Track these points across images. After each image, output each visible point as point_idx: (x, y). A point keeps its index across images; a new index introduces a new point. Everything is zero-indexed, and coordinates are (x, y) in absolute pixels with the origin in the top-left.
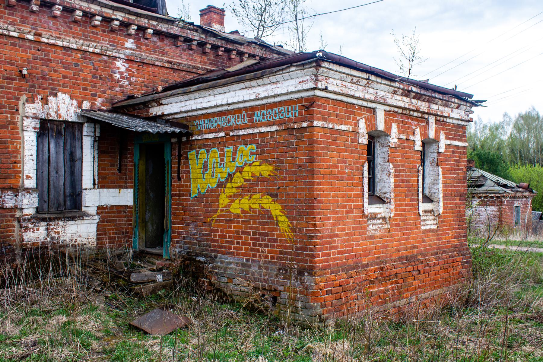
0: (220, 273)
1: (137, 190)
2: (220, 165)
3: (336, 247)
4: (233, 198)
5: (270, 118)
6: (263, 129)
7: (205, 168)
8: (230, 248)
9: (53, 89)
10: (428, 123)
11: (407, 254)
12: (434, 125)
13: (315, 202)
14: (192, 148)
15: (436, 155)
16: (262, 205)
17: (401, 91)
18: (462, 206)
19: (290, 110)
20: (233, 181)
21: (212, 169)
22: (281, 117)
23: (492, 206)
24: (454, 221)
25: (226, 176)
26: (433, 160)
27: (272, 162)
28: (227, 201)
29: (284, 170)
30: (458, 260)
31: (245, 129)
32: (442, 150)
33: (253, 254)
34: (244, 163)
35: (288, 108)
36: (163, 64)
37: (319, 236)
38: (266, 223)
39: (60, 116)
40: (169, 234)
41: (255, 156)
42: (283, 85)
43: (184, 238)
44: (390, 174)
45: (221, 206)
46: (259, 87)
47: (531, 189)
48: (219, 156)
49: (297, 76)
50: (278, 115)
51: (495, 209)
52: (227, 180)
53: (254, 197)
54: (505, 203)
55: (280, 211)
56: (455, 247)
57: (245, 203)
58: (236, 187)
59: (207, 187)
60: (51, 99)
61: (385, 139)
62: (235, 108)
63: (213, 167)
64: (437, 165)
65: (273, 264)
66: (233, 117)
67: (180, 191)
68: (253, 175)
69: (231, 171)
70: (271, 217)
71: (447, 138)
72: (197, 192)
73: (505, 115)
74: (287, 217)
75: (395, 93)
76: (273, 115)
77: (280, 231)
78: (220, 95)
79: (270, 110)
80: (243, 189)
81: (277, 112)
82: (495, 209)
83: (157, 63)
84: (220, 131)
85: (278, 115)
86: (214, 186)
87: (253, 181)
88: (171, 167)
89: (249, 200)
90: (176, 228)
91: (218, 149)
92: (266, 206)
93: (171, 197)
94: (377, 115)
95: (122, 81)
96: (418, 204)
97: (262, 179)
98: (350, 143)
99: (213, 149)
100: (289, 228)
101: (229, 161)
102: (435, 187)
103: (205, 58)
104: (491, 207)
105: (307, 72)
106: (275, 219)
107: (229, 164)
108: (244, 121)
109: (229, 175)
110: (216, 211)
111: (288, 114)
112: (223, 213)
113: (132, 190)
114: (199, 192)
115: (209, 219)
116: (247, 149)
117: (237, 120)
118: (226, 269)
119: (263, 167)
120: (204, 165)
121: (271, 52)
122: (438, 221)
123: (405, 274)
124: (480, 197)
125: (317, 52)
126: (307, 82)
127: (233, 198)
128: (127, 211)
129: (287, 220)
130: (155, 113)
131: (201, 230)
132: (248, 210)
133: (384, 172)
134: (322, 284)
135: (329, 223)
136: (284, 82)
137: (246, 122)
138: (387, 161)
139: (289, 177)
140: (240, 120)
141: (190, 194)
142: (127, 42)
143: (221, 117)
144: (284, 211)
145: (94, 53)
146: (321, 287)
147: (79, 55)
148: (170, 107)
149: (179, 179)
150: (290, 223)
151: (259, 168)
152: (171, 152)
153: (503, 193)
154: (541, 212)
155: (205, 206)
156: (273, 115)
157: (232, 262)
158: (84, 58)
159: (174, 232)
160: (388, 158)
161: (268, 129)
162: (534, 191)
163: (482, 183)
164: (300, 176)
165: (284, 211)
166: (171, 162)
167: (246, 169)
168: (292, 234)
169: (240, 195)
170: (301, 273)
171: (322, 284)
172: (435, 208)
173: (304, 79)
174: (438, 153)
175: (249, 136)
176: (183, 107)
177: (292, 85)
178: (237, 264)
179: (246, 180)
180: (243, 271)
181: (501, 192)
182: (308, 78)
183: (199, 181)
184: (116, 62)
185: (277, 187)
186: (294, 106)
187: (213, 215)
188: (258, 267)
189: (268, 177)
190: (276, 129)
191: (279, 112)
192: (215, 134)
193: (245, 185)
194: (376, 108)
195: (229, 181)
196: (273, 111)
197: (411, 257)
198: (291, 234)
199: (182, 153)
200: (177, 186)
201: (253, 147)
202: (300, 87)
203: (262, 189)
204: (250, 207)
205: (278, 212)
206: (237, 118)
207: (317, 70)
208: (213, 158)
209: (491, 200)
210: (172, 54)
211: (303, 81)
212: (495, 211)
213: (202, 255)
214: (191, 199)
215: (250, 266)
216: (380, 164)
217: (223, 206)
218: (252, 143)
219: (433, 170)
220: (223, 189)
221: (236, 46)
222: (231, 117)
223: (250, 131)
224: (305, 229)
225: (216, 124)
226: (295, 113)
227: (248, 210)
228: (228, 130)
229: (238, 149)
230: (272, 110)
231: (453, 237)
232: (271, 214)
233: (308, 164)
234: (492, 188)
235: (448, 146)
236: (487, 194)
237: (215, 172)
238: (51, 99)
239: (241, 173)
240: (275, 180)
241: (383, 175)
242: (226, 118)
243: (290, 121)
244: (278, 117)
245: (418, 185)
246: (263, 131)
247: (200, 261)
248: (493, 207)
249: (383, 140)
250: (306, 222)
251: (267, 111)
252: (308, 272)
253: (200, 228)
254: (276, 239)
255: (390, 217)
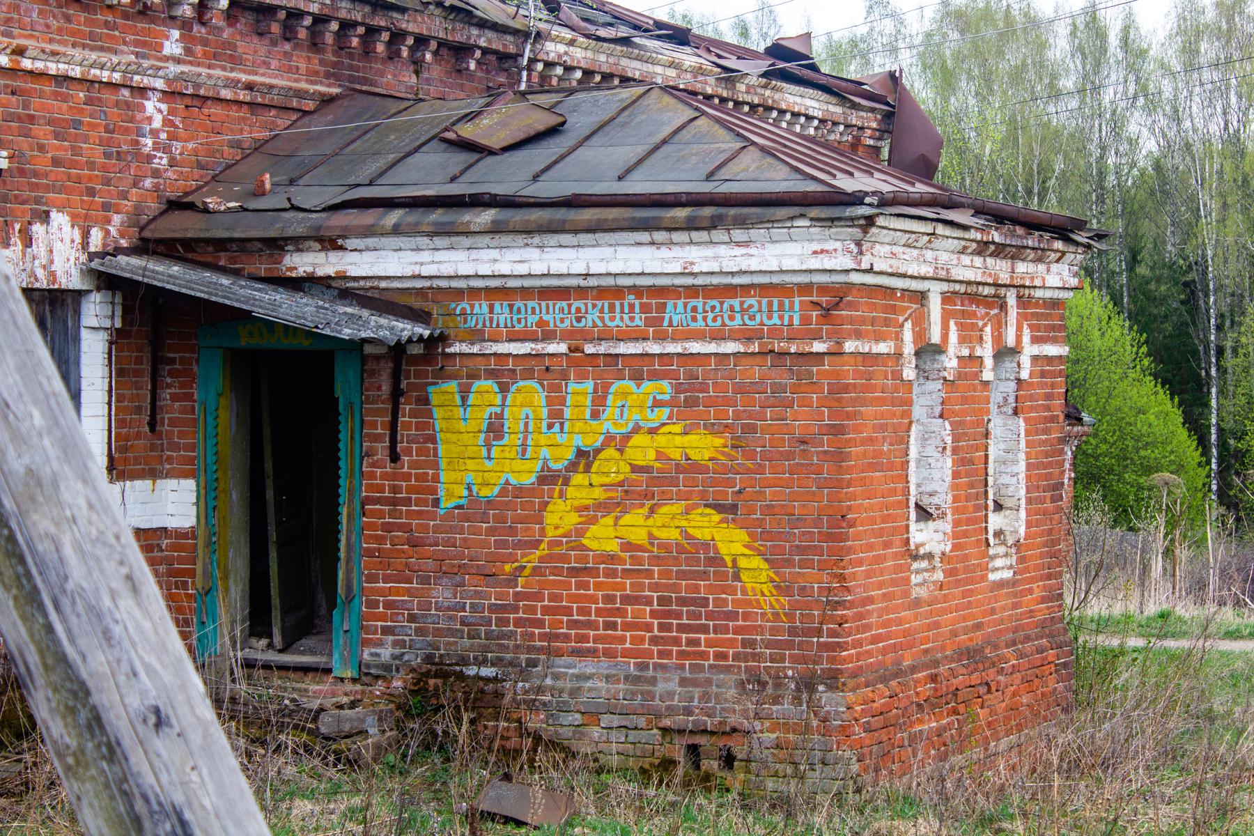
0: (558, 702)
1: (202, 484)
2: (550, 426)
3: (867, 628)
4: (591, 513)
5: (714, 320)
6: (696, 347)
7: (495, 429)
8: (585, 638)
9: (38, 201)
10: (1003, 307)
11: (969, 644)
12: (1015, 311)
13: (844, 524)
14: (442, 375)
15: (1012, 386)
16: (690, 531)
17: (974, 245)
18: (1056, 516)
19: (775, 307)
20: (594, 469)
21: (521, 436)
22: (748, 322)
24: (1042, 556)
25: (570, 455)
26: (1005, 399)
27: (721, 429)
28: (573, 519)
29: (759, 449)
30: (1050, 659)
31: (636, 339)
32: (1025, 375)
33: (659, 652)
34: (631, 425)
35: (770, 304)
36: (235, 93)
37: (849, 601)
38: (704, 575)
39: (52, 275)
40: (356, 610)
41: (666, 411)
42: (766, 252)
43: (412, 618)
44: (944, 448)
45: (551, 533)
46: (694, 248)
48: (544, 403)
49: (809, 237)
50: (738, 316)
52: (572, 467)
53: (664, 510)
55: (745, 546)
56: (1042, 624)
57: (636, 526)
58: (602, 485)
59: (502, 481)
60: (38, 229)
61: (935, 360)
62: (604, 284)
63: (522, 428)
64: (1016, 412)
65: (721, 672)
66: (594, 306)
67: (395, 489)
68: (660, 456)
69: (589, 443)
70: (717, 560)
71: (1035, 340)
72: (466, 493)
74: (766, 560)
75: (963, 251)
76: (726, 316)
77: (744, 592)
78: (563, 249)
79: (715, 302)
80: (626, 492)
81: (737, 308)
83: (226, 94)
84: (549, 336)
85: (738, 316)
86: (529, 479)
87: (659, 470)
88: (362, 421)
89: (648, 517)
90: (381, 592)
91: (543, 386)
92: (702, 534)
93: (363, 507)
94: (931, 307)
95: (155, 156)
96: (986, 516)
97: (691, 467)
98: (890, 382)
99: (521, 384)
100: (771, 585)
101: (581, 417)
102: (1009, 470)
103: (316, 58)
105: (837, 233)
106: (730, 564)
107: (579, 425)
108: (632, 319)
109: (581, 453)
110: (536, 544)
111: (770, 318)
112: (557, 550)
113: (191, 484)
114: (471, 495)
115: (508, 568)
116: (638, 391)
117: (607, 316)
118: (574, 692)
119: (692, 439)
120: (490, 424)
121: (465, 23)
122: (1015, 557)
123: (969, 692)
125: (866, 194)
126: (834, 254)
127: (591, 513)
128: (165, 543)
129: (767, 566)
130: (310, 269)
131: (478, 595)
132: (645, 543)
133: (928, 442)
134: (858, 708)
135: (862, 571)
136: (767, 245)
137: (637, 322)
138: (937, 415)
139: (771, 466)
140: (618, 316)
141: (436, 503)
142: (167, 38)
143: (551, 303)
144: (756, 544)
145: (109, 84)
146: (857, 716)
147: (81, 95)
148: (370, 260)
149: (395, 457)
150: (775, 573)
151: (679, 440)
152: (362, 381)
155: (491, 532)
156: (726, 316)
157: (594, 674)
158: (90, 101)
159: (375, 604)
160: (940, 408)
161: (712, 348)
162: (1086, 417)
164: (803, 465)
165: (756, 544)
166: (362, 408)
167: (637, 440)
168: (781, 599)
169: (618, 504)
170: (807, 684)
171: (858, 708)
172: (1007, 525)
173: (826, 246)
174: (1019, 381)
175: (646, 359)
176: (422, 264)
177: (792, 256)
178: (608, 678)
179: (635, 469)
180: (634, 693)
182: (838, 245)
183: (471, 464)
184: (146, 103)
185: (737, 488)
186: (787, 301)
187: (523, 556)
188: (677, 681)
189: (710, 464)
190: (736, 350)
191: (743, 310)
192: (533, 346)
193: (634, 480)
194: (929, 290)
195: (581, 468)
196: (726, 306)
197: (975, 651)
198: (777, 601)
199: (403, 385)
200: (384, 476)
201: (665, 388)
202: (815, 263)
203: (688, 491)
204: (651, 536)
205: (738, 548)
206: (606, 310)
207: (866, 232)
208: (522, 406)
210: (251, 58)
211: (822, 251)
213: (483, 662)
214: (442, 512)
215: (653, 681)
216: (918, 420)
217: (560, 531)
218: (655, 376)
219: (1005, 425)
220: (558, 488)
221: (392, 18)
222: (586, 305)
223: (655, 348)
224: (816, 586)
225: (533, 319)
226: (791, 318)
227: (645, 543)
228: (576, 337)
229: (613, 389)
230: (722, 304)
231: (1039, 599)
232: (717, 551)
233: (825, 437)
235: (1035, 359)
237: (529, 442)
238: (38, 229)
239: (621, 451)
240: (730, 472)
241: (927, 449)
242: (570, 306)
243: (775, 332)
244: (738, 321)
245: (986, 468)
246: (694, 351)
247: (478, 677)
249: (928, 363)
250: (819, 570)
251: (705, 304)
252: (826, 684)
253: (475, 591)
254: (731, 611)
255: (943, 554)
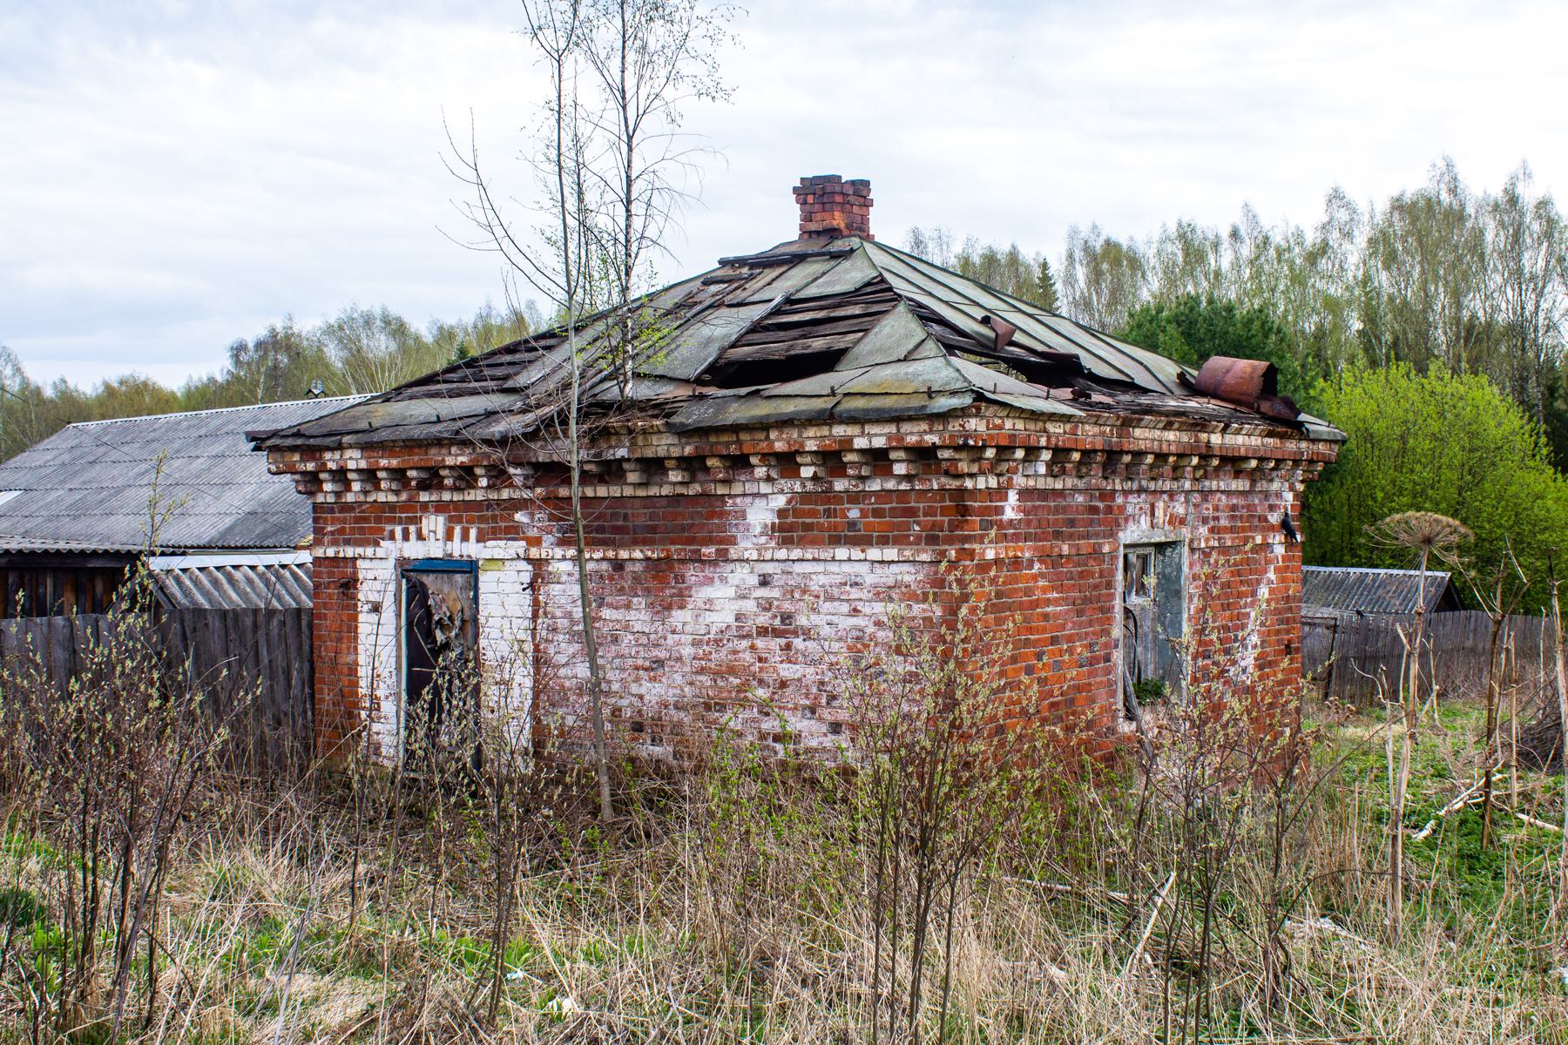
23: (884, 541)
47: (1289, 404)
51: (909, 575)
54: (1009, 514)
73: (1336, 198)
82: (909, 575)
104: (874, 553)
124: (787, 463)
153: (961, 413)
154: (311, 605)
163: (839, 343)
181: (943, 403)
209: (875, 485)
212: (911, 597)
234: (888, 372)
236: (839, 431)
248: (891, 553)
